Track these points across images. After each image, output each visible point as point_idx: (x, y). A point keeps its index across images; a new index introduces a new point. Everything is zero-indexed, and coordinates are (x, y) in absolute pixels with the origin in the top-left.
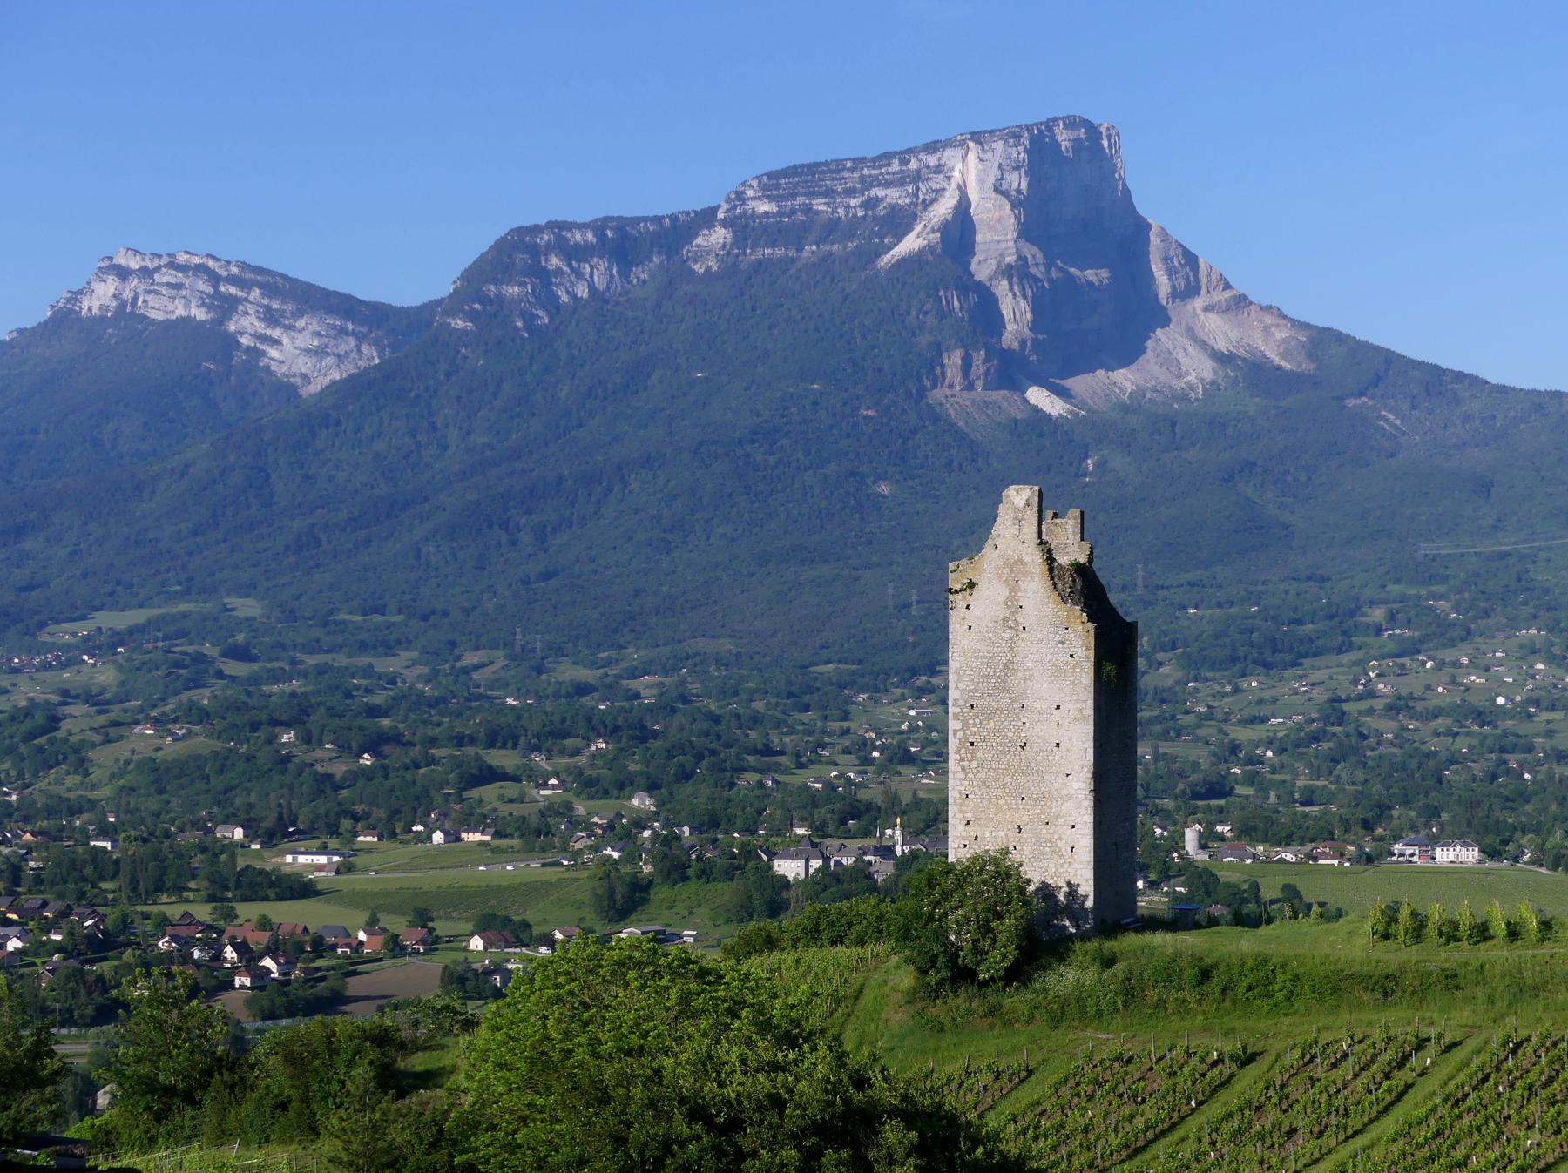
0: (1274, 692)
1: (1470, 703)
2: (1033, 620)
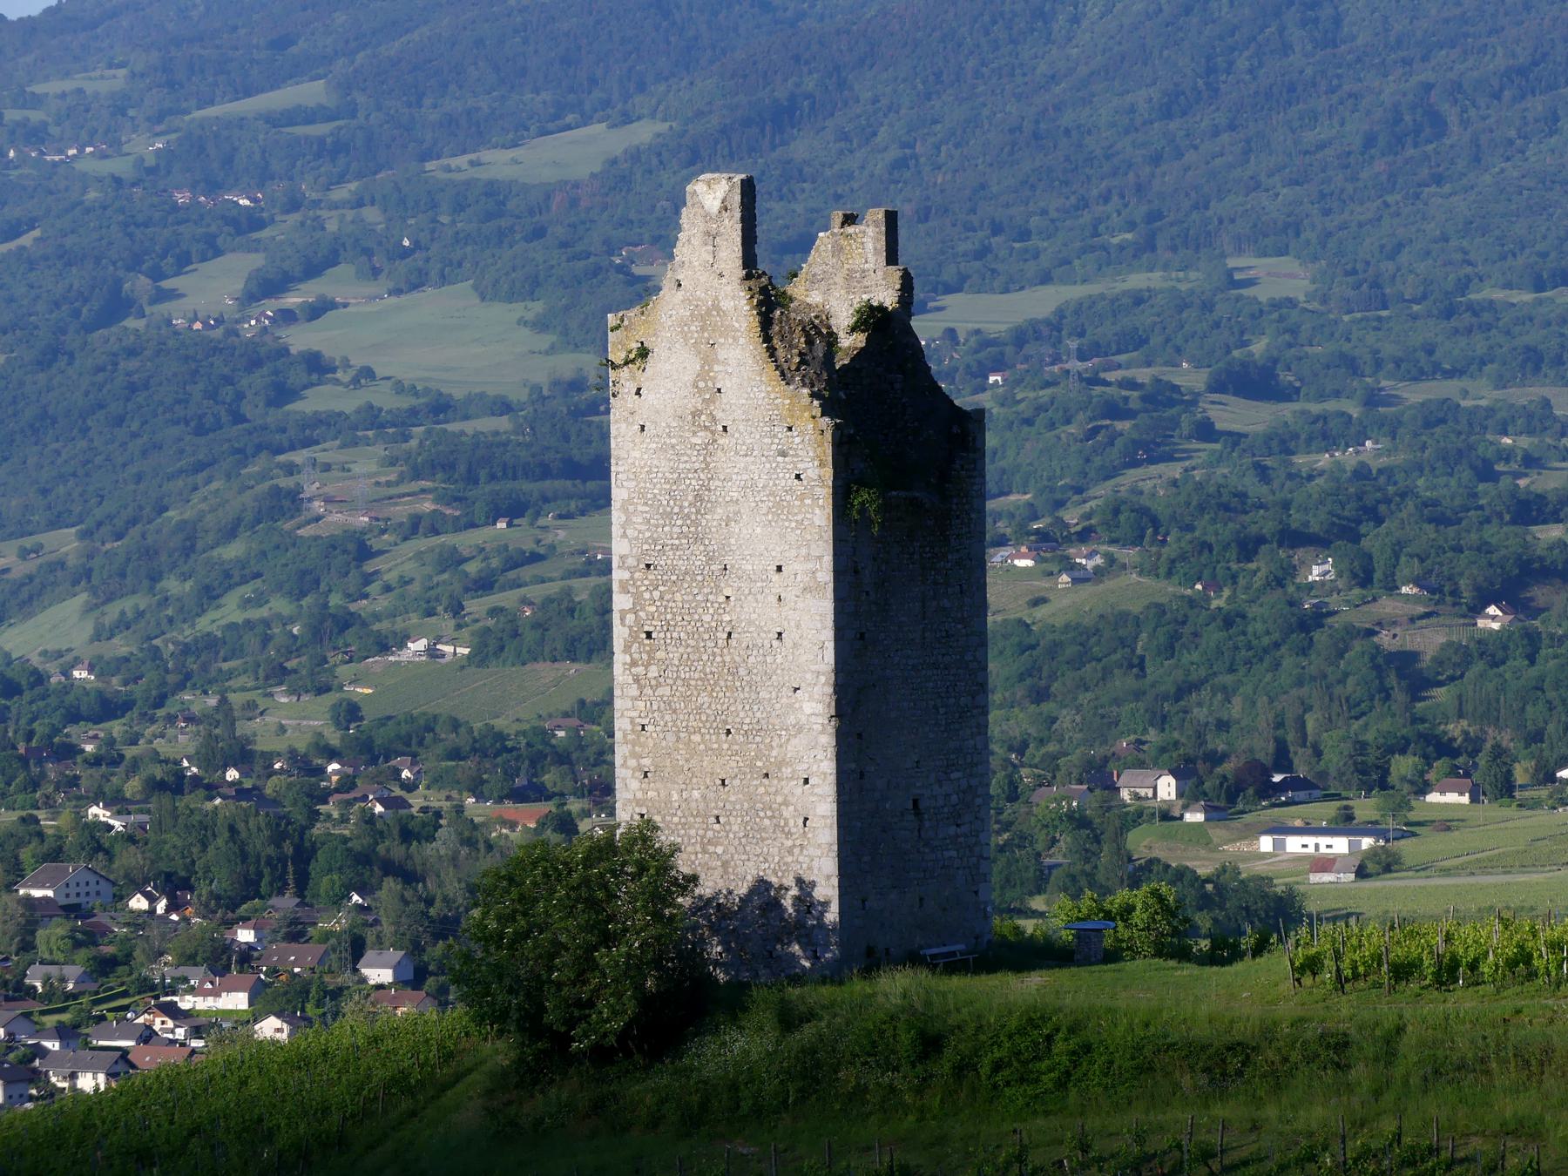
2: (738, 414)
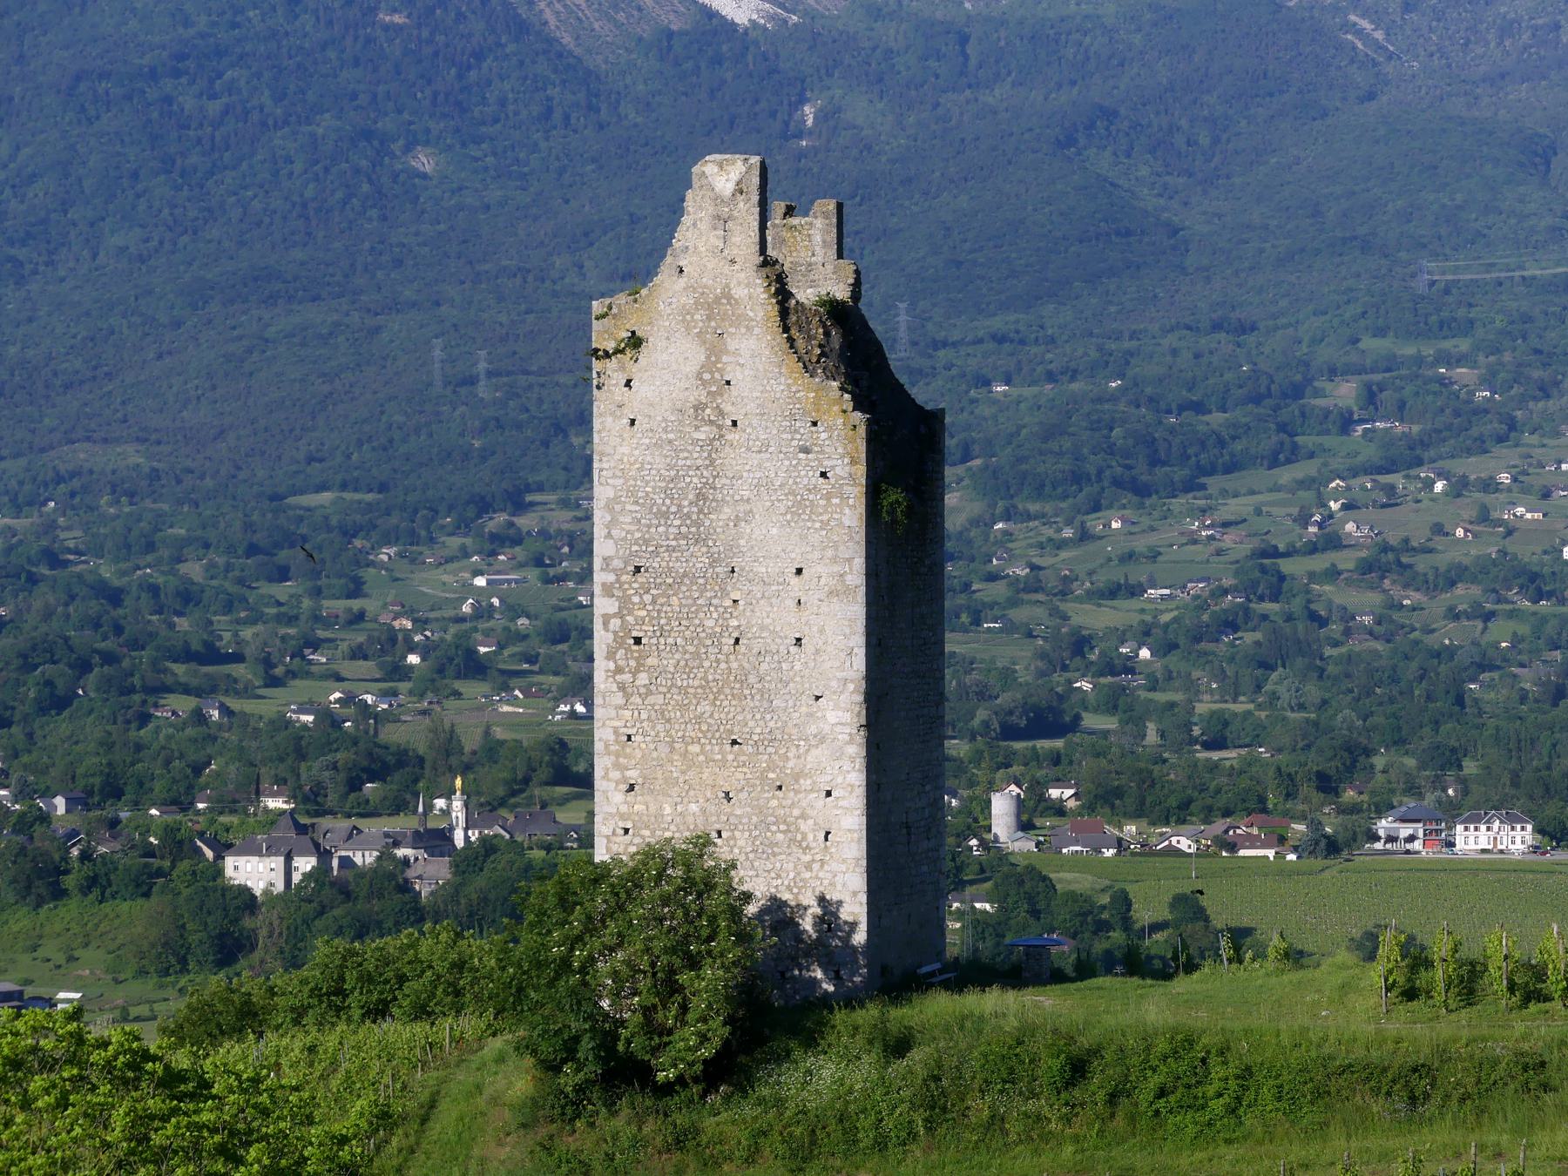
0: (1153, 539)
1: (1515, 556)
2: (751, 407)
